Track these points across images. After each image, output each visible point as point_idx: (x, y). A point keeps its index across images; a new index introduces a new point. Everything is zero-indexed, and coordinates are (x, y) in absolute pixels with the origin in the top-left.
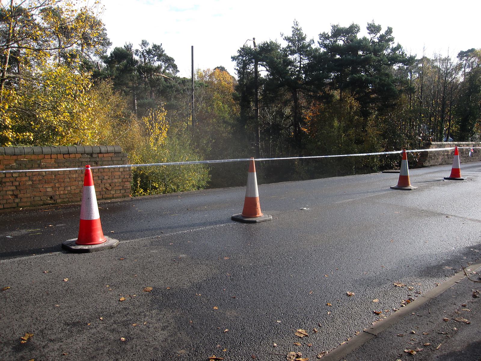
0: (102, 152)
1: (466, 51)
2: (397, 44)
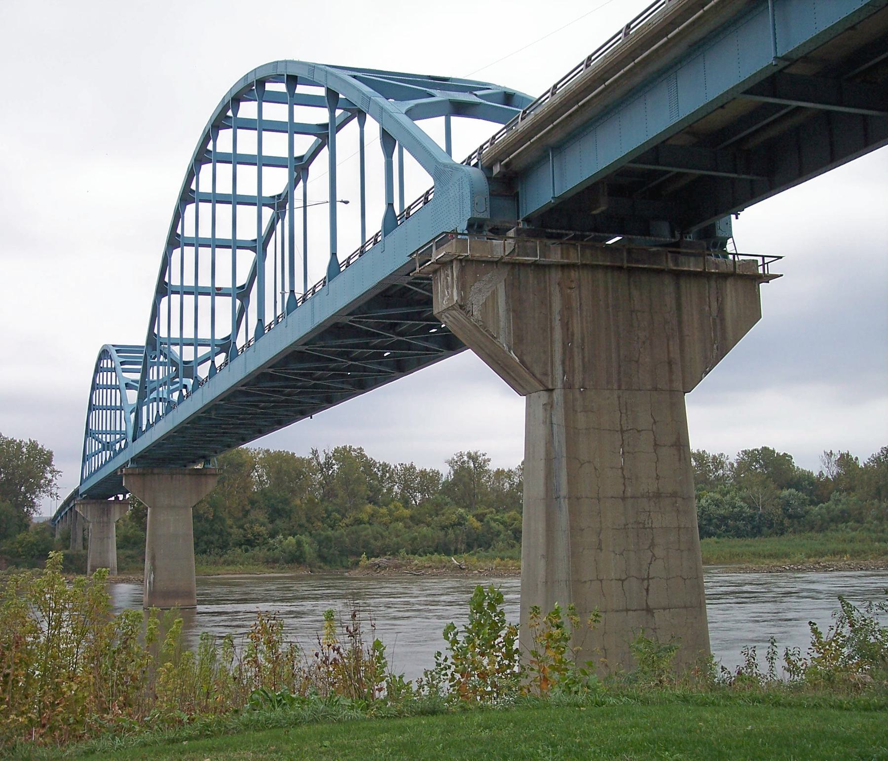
0: (537, 97)
1: (523, 459)
2: (484, 453)
